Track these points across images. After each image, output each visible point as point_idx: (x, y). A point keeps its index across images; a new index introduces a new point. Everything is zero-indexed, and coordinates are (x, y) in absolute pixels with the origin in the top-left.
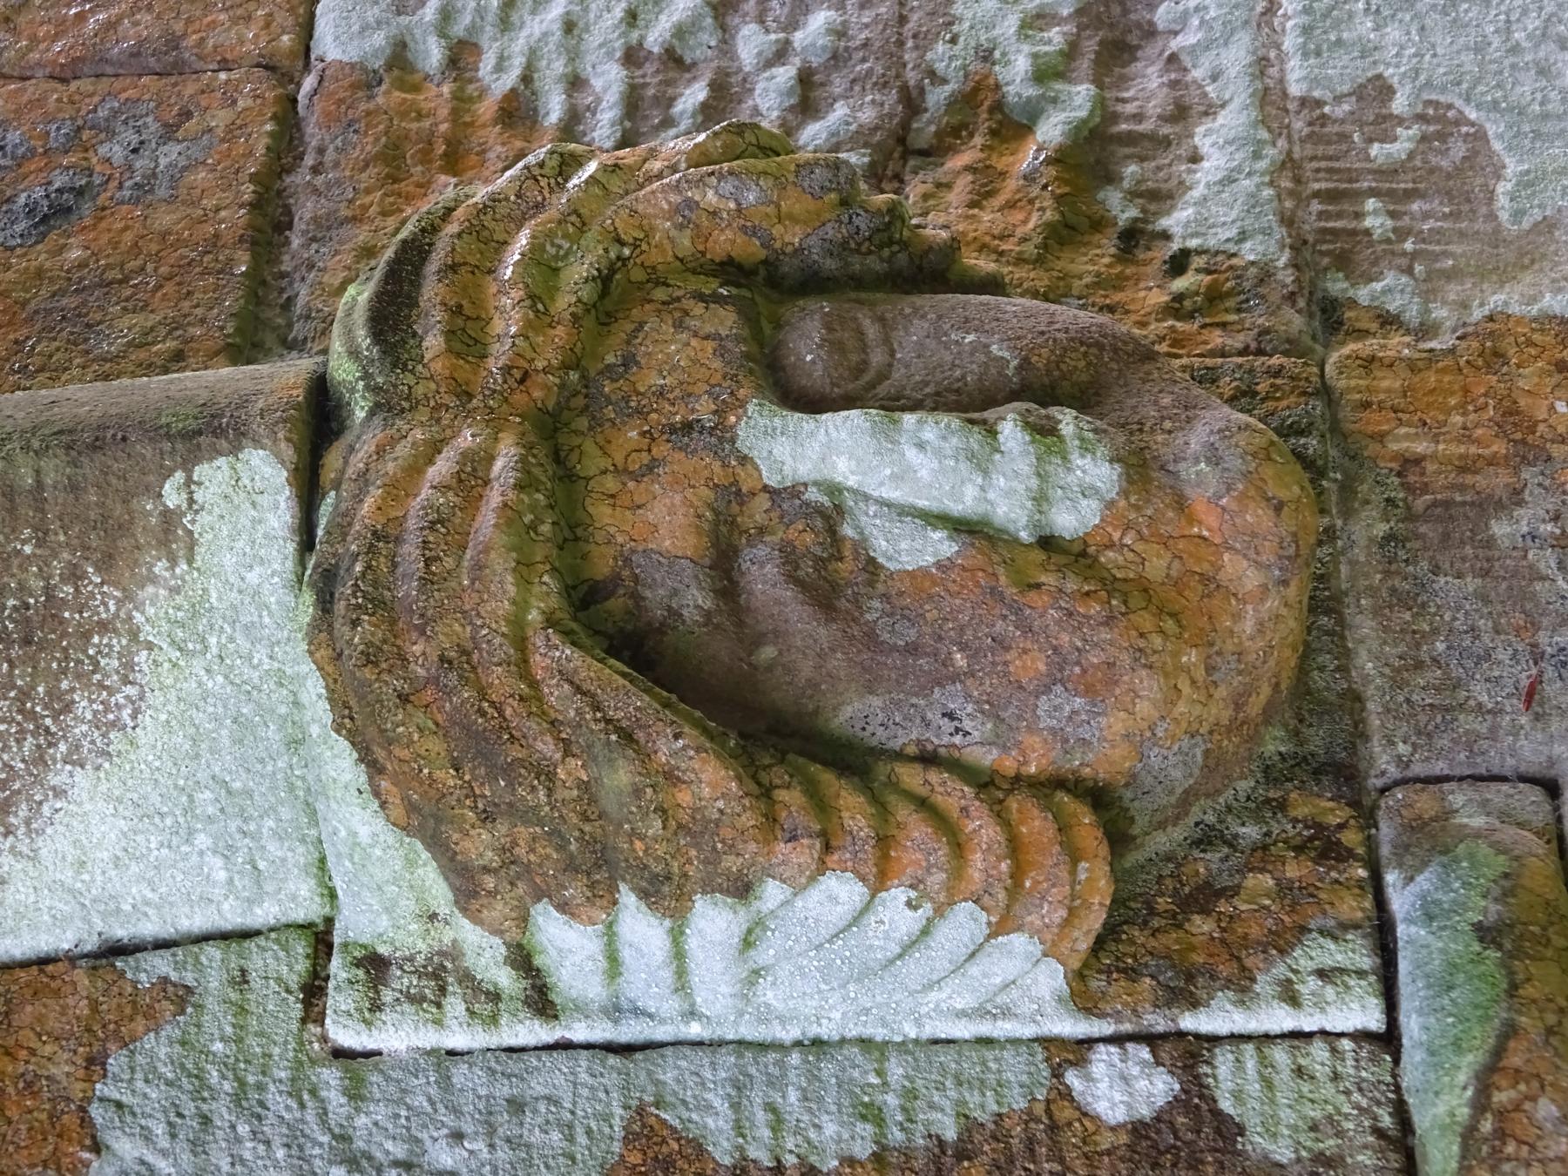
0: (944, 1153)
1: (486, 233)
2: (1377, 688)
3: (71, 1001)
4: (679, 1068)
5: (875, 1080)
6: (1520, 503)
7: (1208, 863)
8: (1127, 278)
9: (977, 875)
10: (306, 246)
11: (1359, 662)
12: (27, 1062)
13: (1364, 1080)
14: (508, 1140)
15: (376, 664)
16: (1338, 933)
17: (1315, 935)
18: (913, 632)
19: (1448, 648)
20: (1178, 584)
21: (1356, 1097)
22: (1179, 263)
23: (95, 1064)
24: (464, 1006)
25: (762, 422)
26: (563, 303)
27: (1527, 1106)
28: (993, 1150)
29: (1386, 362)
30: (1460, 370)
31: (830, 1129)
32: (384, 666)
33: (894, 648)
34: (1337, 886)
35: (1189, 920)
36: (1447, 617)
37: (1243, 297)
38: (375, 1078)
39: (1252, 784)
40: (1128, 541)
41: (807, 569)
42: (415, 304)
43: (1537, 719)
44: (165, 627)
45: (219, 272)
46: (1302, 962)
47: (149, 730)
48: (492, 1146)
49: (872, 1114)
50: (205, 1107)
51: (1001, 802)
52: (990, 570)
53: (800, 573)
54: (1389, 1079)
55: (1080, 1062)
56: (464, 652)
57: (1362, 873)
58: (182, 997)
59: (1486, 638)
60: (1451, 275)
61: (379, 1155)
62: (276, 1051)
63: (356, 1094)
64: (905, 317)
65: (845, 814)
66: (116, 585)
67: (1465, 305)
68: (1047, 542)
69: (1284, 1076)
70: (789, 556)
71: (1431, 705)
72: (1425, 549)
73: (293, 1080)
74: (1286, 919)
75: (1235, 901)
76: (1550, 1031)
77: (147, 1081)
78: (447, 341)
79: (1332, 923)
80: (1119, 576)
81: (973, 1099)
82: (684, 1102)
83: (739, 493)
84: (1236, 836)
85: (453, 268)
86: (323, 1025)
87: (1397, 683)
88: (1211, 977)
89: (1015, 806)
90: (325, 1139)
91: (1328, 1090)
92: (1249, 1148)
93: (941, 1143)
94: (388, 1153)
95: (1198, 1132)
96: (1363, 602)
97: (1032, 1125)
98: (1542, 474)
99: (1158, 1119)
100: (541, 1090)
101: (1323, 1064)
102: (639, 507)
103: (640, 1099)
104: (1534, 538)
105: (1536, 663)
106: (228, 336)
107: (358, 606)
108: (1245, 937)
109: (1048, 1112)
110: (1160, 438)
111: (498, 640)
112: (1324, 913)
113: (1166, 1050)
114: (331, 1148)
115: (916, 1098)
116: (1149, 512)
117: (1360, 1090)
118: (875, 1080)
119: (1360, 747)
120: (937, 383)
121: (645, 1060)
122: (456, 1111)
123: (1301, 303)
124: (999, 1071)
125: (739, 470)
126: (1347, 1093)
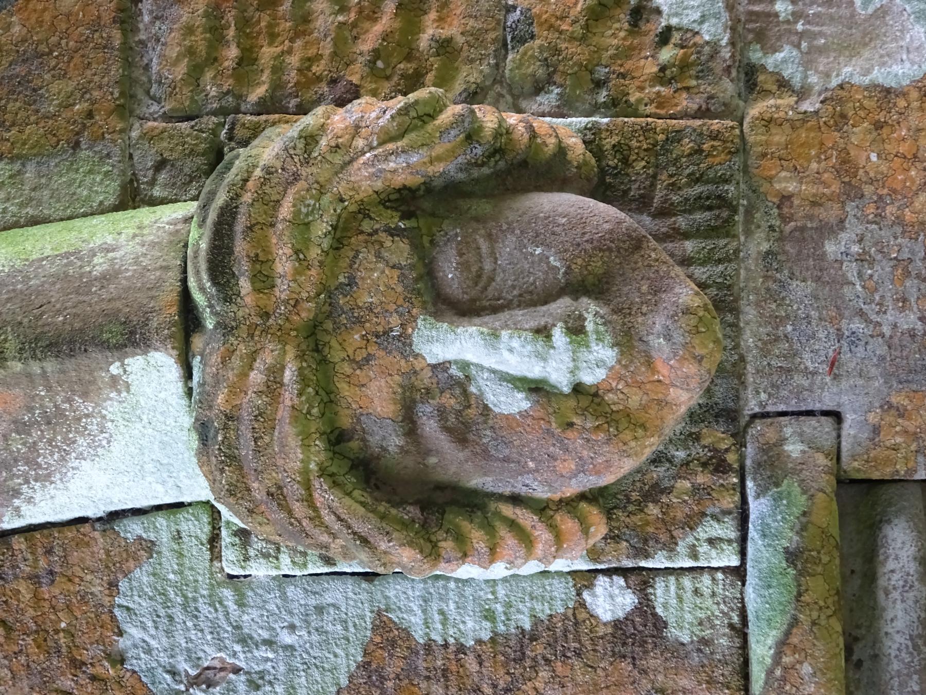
0: (524, 637)
1: (266, 198)
2: (753, 357)
3: (95, 549)
4: (396, 589)
5: (490, 596)
6: (843, 229)
7: (659, 472)
8: (634, 49)
9: (540, 552)
10: (152, 23)
11: (745, 337)
12: (80, 585)
13: (727, 596)
14: (317, 630)
15: (235, 495)
16: (720, 516)
17: (709, 518)
18: (507, 451)
19: (794, 330)
20: (644, 408)
21: (722, 606)
22: (665, 37)
23: (113, 585)
24: (290, 560)
25: (426, 333)
26: (314, 253)
27: (798, 666)
28: (548, 636)
29: (779, 122)
30: (820, 128)
31: (470, 624)
32: (239, 495)
33: (498, 459)
34: (722, 489)
35: (647, 506)
36: (795, 307)
37: (700, 68)
38: (250, 593)
39: (684, 425)
40: (620, 387)
41: (452, 419)
42: (231, 253)
43: (835, 378)
44: (119, 414)
45: (105, 47)
46: (701, 534)
47: (116, 447)
48: (309, 632)
49: (489, 615)
50: (169, 611)
51: (552, 517)
52: (547, 419)
53: (449, 423)
54: (739, 596)
55: (590, 586)
56: (280, 488)
57: (735, 480)
58: (150, 547)
59: (814, 323)
60: (821, 50)
61: (255, 636)
62: (200, 579)
63: (241, 604)
64: (503, 232)
65: (474, 541)
66: (91, 402)
67: (828, 75)
68: (578, 389)
69: (688, 595)
70: (442, 413)
71: (781, 367)
72: (788, 260)
73: (210, 596)
74: (695, 508)
75: (671, 496)
76: (814, 623)
77: (140, 596)
78: (253, 283)
79: (718, 510)
80: (614, 409)
81: (538, 607)
82: (400, 608)
83: (415, 372)
84: (673, 456)
85: (250, 228)
86: (221, 561)
87: (765, 352)
88: (656, 541)
89: (559, 518)
90: (229, 629)
91: (709, 602)
92: (669, 635)
93: (523, 631)
94: (259, 635)
95: (645, 626)
96: (751, 297)
97: (566, 622)
98: (857, 207)
99: (626, 619)
100: (330, 601)
101: (708, 588)
102: (363, 386)
103: (378, 607)
104: (847, 255)
105: (839, 342)
106: (117, 99)
107: (222, 462)
108: (674, 518)
109: (574, 614)
110: (640, 320)
111: (296, 487)
112: (714, 505)
113: (633, 579)
114: (233, 634)
115: (511, 607)
116: (632, 369)
117: (724, 602)
118: (490, 596)
119: (742, 392)
120: (521, 288)
121: (380, 585)
122: (291, 613)
123: (734, 73)
124: (551, 591)
125: (415, 362)
126: (718, 604)
